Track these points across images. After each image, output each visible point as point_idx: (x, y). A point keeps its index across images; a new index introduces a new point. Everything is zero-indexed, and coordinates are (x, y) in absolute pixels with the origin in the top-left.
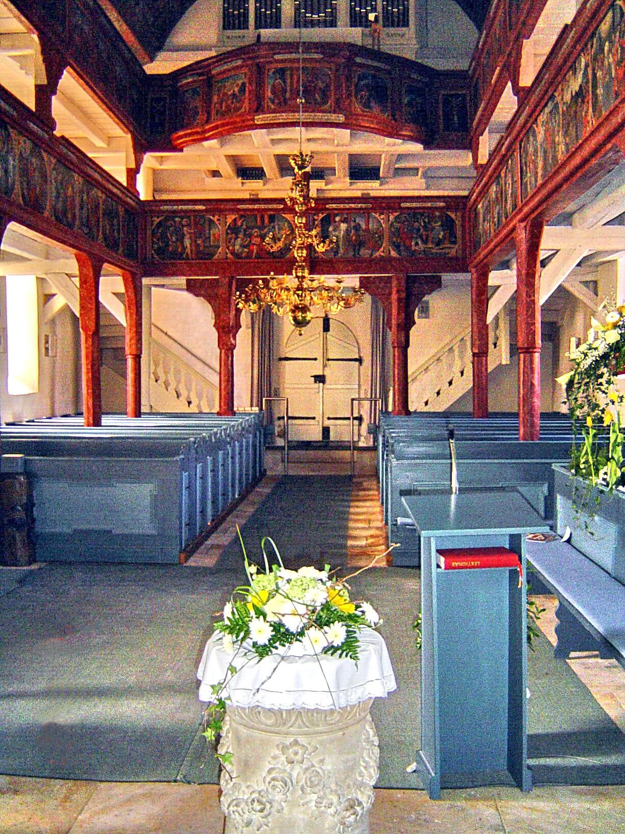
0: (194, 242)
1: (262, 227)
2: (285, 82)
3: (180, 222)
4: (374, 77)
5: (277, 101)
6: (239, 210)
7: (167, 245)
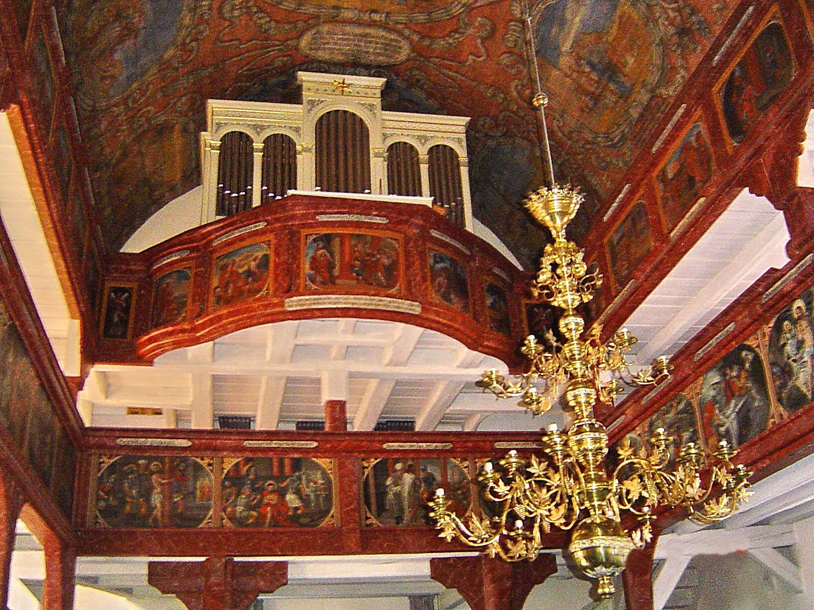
0: (167, 498)
1: (281, 477)
2: (332, 254)
3: (147, 467)
4: (453, 262)
5: (319, 279)
6: (245, 449)
7: (123, 502)
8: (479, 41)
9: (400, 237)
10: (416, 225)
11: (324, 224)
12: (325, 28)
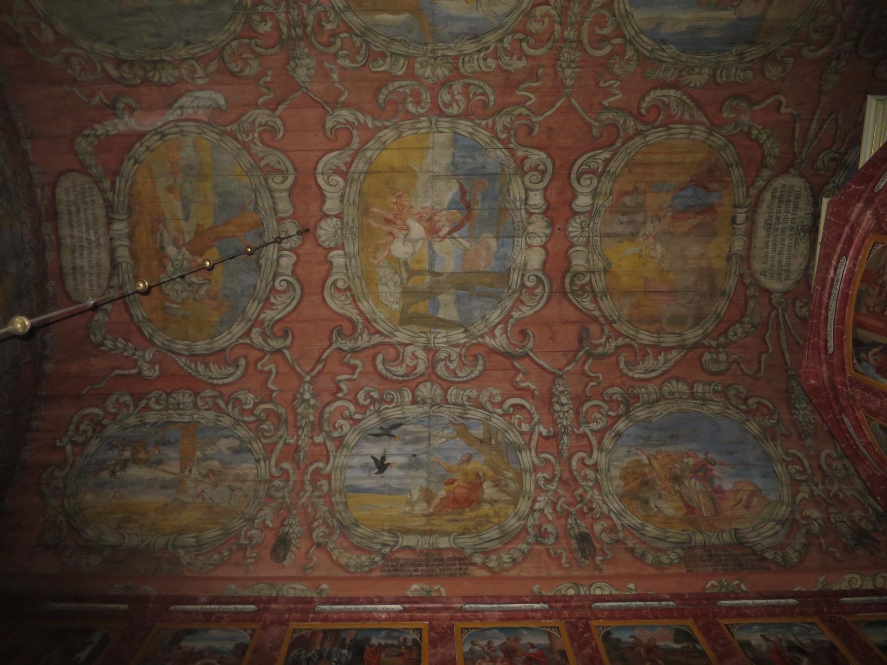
2: (874, 344)
8: (756, 108)
9: (869, 243)
10: (862, 212)
11: (839, 344)
12: (757, 266)
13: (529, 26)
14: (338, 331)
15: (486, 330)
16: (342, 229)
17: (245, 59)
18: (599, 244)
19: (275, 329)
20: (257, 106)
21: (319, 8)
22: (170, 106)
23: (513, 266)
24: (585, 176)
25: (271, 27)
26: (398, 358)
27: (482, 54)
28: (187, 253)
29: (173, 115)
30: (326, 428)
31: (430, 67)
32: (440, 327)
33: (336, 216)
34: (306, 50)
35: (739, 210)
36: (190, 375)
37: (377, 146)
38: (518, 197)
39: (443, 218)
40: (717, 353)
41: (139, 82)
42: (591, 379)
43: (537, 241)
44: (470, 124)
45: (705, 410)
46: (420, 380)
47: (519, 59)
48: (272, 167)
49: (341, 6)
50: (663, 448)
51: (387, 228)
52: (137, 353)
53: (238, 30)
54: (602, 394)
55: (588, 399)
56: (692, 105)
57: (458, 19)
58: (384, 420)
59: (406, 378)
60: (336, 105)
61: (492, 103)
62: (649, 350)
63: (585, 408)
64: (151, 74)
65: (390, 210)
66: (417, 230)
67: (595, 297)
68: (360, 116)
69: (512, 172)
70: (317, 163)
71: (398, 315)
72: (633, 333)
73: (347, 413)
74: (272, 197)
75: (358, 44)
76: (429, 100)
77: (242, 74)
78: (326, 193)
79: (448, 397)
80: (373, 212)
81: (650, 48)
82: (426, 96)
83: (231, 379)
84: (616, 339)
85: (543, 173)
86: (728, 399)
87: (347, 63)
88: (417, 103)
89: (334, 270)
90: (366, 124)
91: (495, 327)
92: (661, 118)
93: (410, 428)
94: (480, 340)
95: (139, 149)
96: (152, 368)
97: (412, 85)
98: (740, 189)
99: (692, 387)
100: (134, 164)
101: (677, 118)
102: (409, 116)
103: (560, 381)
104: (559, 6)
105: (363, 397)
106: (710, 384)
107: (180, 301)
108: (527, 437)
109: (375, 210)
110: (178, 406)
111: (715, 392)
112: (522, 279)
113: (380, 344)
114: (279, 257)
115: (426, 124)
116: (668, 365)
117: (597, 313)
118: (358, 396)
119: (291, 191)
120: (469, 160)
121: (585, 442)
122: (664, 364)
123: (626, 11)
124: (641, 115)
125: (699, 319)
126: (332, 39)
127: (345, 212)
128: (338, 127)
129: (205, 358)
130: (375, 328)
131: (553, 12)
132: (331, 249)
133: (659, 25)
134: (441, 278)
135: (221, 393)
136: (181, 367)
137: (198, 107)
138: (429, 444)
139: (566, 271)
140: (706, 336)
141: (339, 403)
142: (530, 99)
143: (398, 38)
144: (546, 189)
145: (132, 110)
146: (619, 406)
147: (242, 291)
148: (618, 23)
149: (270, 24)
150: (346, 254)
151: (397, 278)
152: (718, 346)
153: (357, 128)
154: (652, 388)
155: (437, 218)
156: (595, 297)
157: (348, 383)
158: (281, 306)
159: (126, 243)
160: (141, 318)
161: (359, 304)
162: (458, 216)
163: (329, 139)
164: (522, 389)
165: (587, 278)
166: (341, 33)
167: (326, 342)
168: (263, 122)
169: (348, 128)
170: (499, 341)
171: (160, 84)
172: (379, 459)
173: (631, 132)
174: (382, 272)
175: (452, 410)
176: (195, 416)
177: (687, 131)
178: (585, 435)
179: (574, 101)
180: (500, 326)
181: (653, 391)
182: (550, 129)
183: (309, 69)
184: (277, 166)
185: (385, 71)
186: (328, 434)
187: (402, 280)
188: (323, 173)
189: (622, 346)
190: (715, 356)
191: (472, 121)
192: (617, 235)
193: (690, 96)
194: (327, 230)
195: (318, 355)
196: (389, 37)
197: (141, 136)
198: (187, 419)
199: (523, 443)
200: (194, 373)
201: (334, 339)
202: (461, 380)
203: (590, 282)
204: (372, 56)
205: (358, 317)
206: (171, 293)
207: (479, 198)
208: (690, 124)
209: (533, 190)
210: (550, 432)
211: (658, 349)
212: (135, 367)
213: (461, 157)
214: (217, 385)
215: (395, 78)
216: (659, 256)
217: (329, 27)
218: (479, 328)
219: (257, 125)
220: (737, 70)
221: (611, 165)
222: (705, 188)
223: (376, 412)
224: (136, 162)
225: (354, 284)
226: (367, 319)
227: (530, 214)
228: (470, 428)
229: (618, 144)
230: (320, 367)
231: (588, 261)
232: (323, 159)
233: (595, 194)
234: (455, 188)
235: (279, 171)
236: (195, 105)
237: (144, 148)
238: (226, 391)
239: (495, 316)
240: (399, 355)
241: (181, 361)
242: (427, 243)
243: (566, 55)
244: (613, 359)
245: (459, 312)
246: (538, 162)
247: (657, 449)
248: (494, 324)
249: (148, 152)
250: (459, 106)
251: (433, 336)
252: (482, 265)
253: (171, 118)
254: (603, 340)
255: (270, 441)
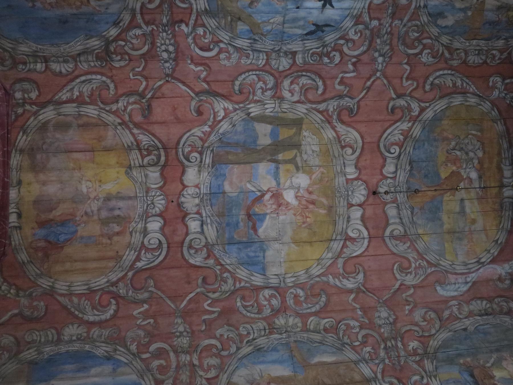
8: (16, 311)
13: (218, 361)
14: (352, 113)
15: (232, 115)
16: (348, 195)
17: (425, 320)
18: (138, 191)
19: (401, 114)
20: (414, 287)
21: (377, 362)
22: (474, 283)
23: (210, 170)
24: (155, 246)
25: (409, 345)
26: (305, 90)
27: (251, 337)
28: (463, 174)
29: (473, 277)
30: (368, 32)
31: (290, 324)
32: (270, 117)
33: (353, 205)
34: (382, 330)
35: (16, 224)
36: (467, 77)
37: (324, 261)
38: (209, 226)
39: (269, 206)
40: (24, 99)
41: (496, 300)
42: (140, 74)
43: (191, 191)
44: (253, 283)
45: (34, 46)
46: (288, 72)
47: (221, 335)
48: (401, 242)
49: (361, 364)
50: (75, 11)
51: (314, 197)
52: (504, 95)
53: (431, 342)
54: (130, 60)
55: (143, 56)
56: (73, 310)
57: (274, 362)
58: (320, 39)
59: (300, 74)
60: (358, 291)
61: (238, 300)
62: (87, 99)
63: (146, 48)
64: (488, 305)
65: (311, 212)
66: (289, 196)
67: (138, 145)
68: (338, 283)
69: (216, 247)
70: (368, 247)
71: (304, 126)
72: (104, 115)
73: (350, 45)
74: (401, 219)
75: (346, 338)
76: (287, 299)
77: (425, 310)
78: (361, 223)
79: (265, 57)
80: (325, 209)
81: (118, 352)
82: (290, 302)
83: (438, 74)
84: (118, 109)
85: (190, 247)
86: (11, 57)
87: (353, 323)
88: (296, 296)
89: (354, 162)
90: (333, 278)
91: (224, 118)
92: (97, 298)
93: (299, 32)
94: (237, 107)
95: (495, 251)
96: (494, 83)
97: (302, 310)
98: (17, 243)
99: (47, 67)
100: (498, 239)
101: (84, 299)
102: (302, 286)
103: (168, 71)
104: (198, 379)
105: (336, 58)
106: (29, 70)
107: (470, 136)
108: (200, 22)
109: (323, 212)
110: (479, 52)
111: (25, 63)
112: (202, 159)
113: (319, 103)
114: (396, 172)
115: (288, 280)
116: (69, 87)
117: (135, 131)
118: (339, 59)
119: (387, 224)
120: (252, 254)
121: (147, 17)
122: (73, 88)
123: (144, 380)
124: (113, 298)
125: (44, 127)
126: (365, 340)
127: (346, 209)
128: (355, 275)
129: (456, 91)
130: (323, 116)
131: (201, 373)
132: (356, 179)
133: (114, 370)
134: (269, 158)
135: (446, 62)
136: (473, 83)
137: (455, 284)
138: (284, 17)
139: (164, 166)
140: (36, 114)
141: (356, 53)
142: (209, 305)
143: (317, 344)
144: (187, 234)
145: (500, 279)
146: (115, 50)
147: (424, 144)
148: (149, 370)
149: (410, 348)
150: (345, 176)
151: (305, 157)
152: (23, 105)
153: (340, 275)
154: (84, 67)
155: (274, 207)
156: (138, 145)
157: (347, 70)
158: (395, 133)
159: (505, 180)
160: (499, 122)
161: (335, 135)
162: (257, 209)
163: (360, 265)
164: (201, 64)
165: (146, 160)
166: (359, 345)
167: (362, 103)
168: (409, 275)
169: (347, 274)
170: (220, 106)
171: (481, 299)
172: (328, 6)
173: (121, 284)
174: (317, 162)
175: (263, 46)
176: (468, 44)
177: (73, 288)
178: (147, 23)
179: (173, 306)
180: (220, 118)
181: (84, 64)
182: (189, 283)
183: (379, 317)
184: (398, 242)
185: (324, 319)
186: (367, 28)
187: (301, 156)
188: (364, 238)
189: (113, 103)
190: (26, 96)
191: (252, 285)
192: (123, 198)
193: (77, 317)
194: (360, 194)
195: (370, 93)
196: (324, 344)
197: (493, 261)
198: (474, 42)
199: (203, 17)
200: (465, 79)
201: (356, 107)
202: (254, 73)
203: (143, 159)
204: (334, 329)
205: (336, 124)
206: (476, 142)
207: (241, 224)
208: (71, 294)
209: (197, 233)
210: (179, 27)
211: (80, 101)
212: (507, 84)
213: (258, 257)
214: (449, 69)
215: (315, 314)
216: (83, 182)
217: (368, 349)
218: (238, 117)
219: (413, 272)
220: (40, 341)
221: (134, 257)
222: (49, 242)
223: (326, 46)
224: (497, 241)
225: (339, 152)
226: (329, 123)
227: (198, 213)
228: (248, 31)
229: (130, 274)
230: (369, 83)
231: (146, 176)
232: (364, 249)
233: (145, 232)
234: (260, 231)
235: (396, 238)
236: (457, 286)
237: (492, 252)
238: (442, 65)
239: (225, 126)
240: (305, 93)
241: (472, 89)
242: (281, 186)
243: (185, 342)
244: (120, 92)
245: (254, 130)
246: (196, 256)
247: (81, 10)
248: (225, 120)
249: (488, 249)
250: (264, 297)
251: (275, 110)
252: (236, 169)
253: (473, 275)
254: (130, 107)
255: (414, 22)
